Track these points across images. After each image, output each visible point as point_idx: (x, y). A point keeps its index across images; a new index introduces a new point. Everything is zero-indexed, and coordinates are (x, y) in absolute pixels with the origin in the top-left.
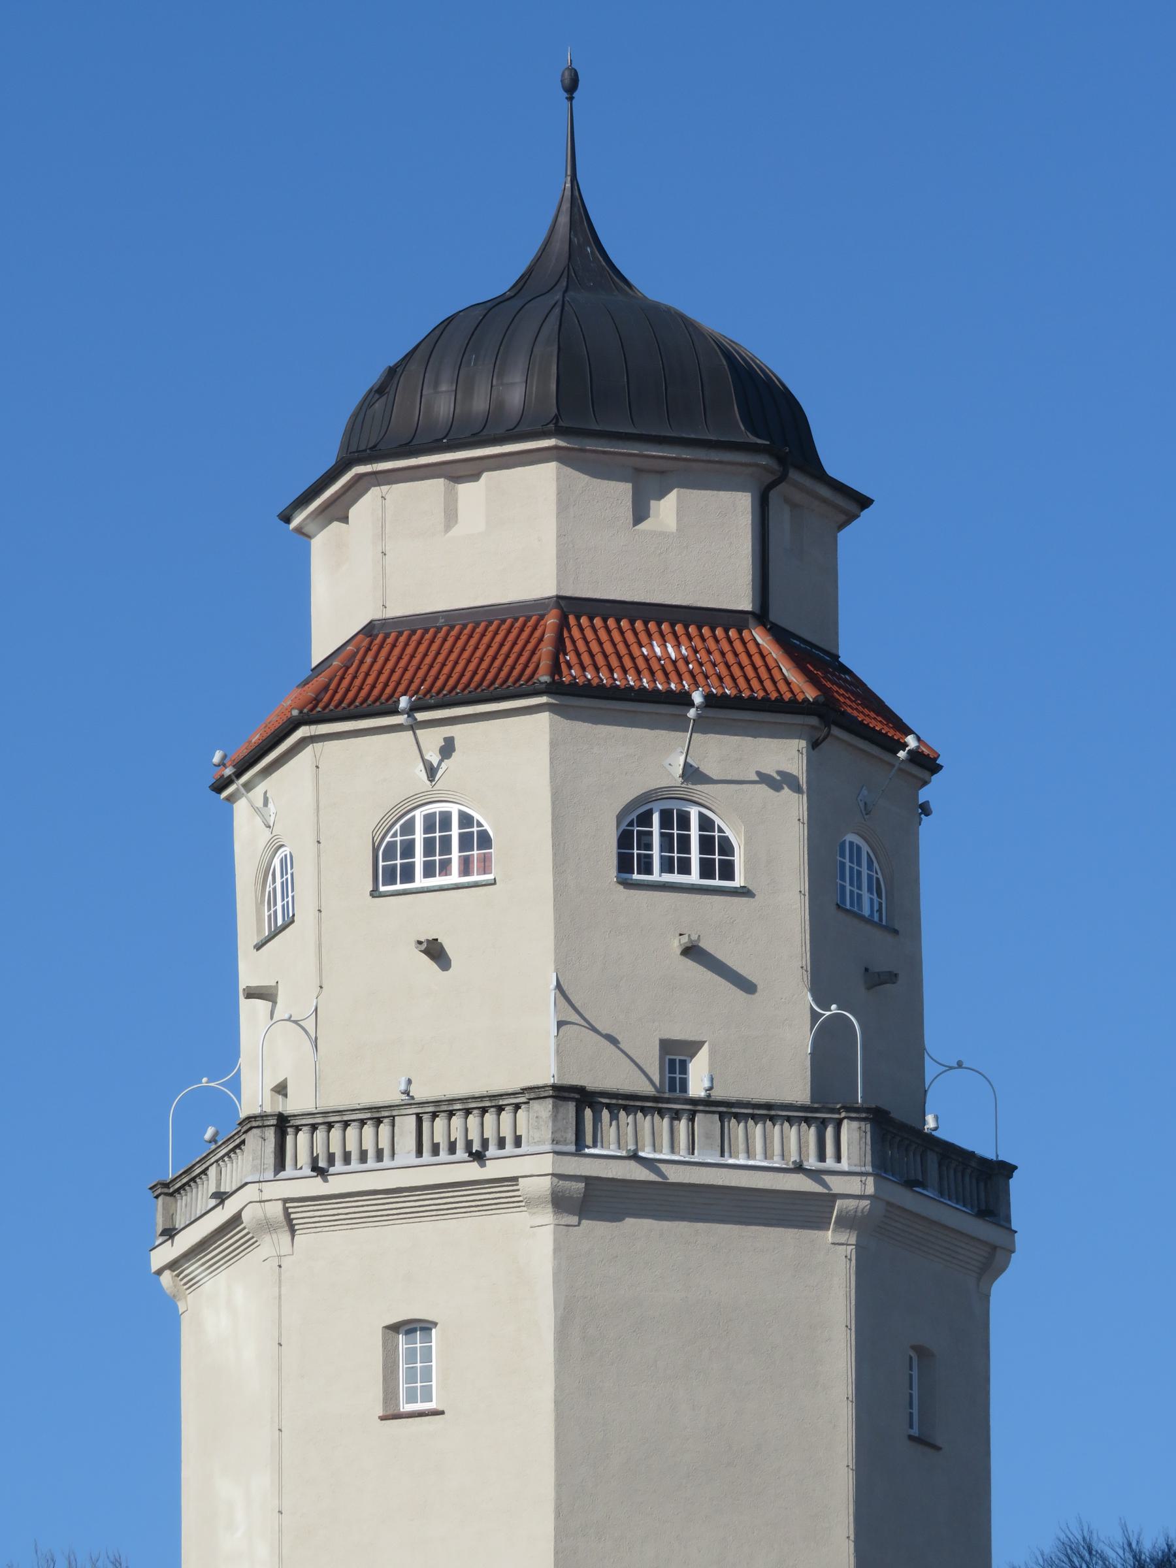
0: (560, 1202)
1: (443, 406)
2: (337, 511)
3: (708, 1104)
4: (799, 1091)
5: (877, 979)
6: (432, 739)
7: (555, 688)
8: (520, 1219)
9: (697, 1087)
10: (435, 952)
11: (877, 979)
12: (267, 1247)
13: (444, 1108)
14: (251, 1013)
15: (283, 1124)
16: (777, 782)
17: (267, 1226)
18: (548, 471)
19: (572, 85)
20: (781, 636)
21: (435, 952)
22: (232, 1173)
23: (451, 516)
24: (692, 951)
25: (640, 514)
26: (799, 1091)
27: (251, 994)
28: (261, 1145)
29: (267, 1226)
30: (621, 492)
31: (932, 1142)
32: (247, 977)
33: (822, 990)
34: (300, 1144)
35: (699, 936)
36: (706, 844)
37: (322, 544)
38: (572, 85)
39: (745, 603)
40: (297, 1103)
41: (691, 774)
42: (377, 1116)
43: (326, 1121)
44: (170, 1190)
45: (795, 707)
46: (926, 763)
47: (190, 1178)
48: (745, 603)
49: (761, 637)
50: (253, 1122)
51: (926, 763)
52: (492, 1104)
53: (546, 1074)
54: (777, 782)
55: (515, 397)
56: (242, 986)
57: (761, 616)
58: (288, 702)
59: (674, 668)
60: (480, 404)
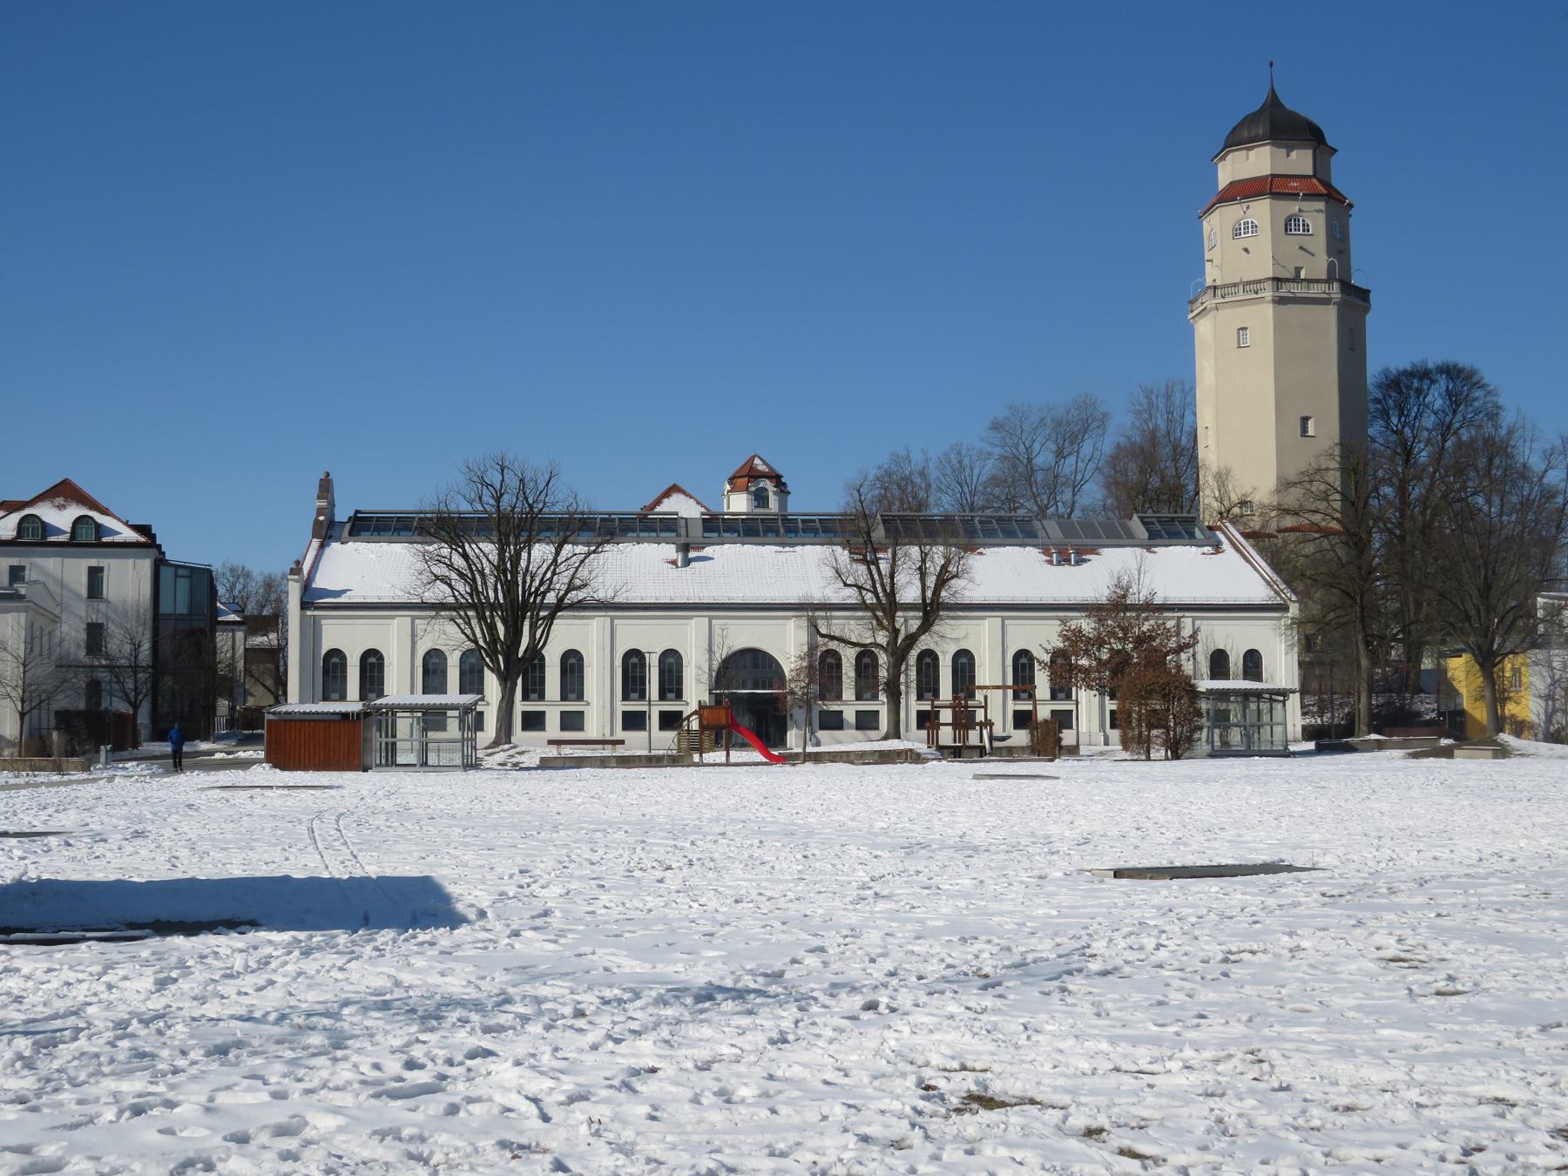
0: (1274, 302)
1: (1245, 134)
2: (1223, 158)
3: (1305, 280)
4: (1324, 276)
5: (1341, 252)
6: (1245, 205)
7: (1271, 193)
8: (1266, 305)
9: (1303, 276)
10: (1246, 250)
11: (1341, 252)
12: (1212, 314)
13: (1249, 283)
14: (1208, 265)
15: (1215, 288)
16: (1319, 211)
17: (1212, 309)
18: (1268, 147)
19: (1271, 65)
20: (1319, 180)
21: (1246, 250)
22: (1205, 298)
23: (1248, 158)
24: (1301, 248)
25: (1288, 156)
26: (1324, 276)
27: (95, 574)
28: (1211, 292)
29: (1212, 309)
30: (1283, 151)
31: (1353, 286)
32: (1206, 258)
33: (1329, 255)
34: (1219, 292)
35: (653, 1070)
37: (1220, 166)
38: (1271, 65)
39: (1310, 173)
40: (1218, 283)
41: (1300, 210)
42: (1235, 285)
43: (1224, 287)
44: (1191, 302)
45: (1322, 195)
46: (1351, 206)
47: (1195, 300)
48: (1310, 173)
49: (1314, 181)
50: (1209, 287)
51: (1351, 206)
52: (1259, 281)
53: (1271, 275)
54: (1319, 211)
55: (1261, 132)
56: (103, 563)
57: (1314, 176)
58: (1214, 198)
59: (1296, 188)
60: (1253, 134)
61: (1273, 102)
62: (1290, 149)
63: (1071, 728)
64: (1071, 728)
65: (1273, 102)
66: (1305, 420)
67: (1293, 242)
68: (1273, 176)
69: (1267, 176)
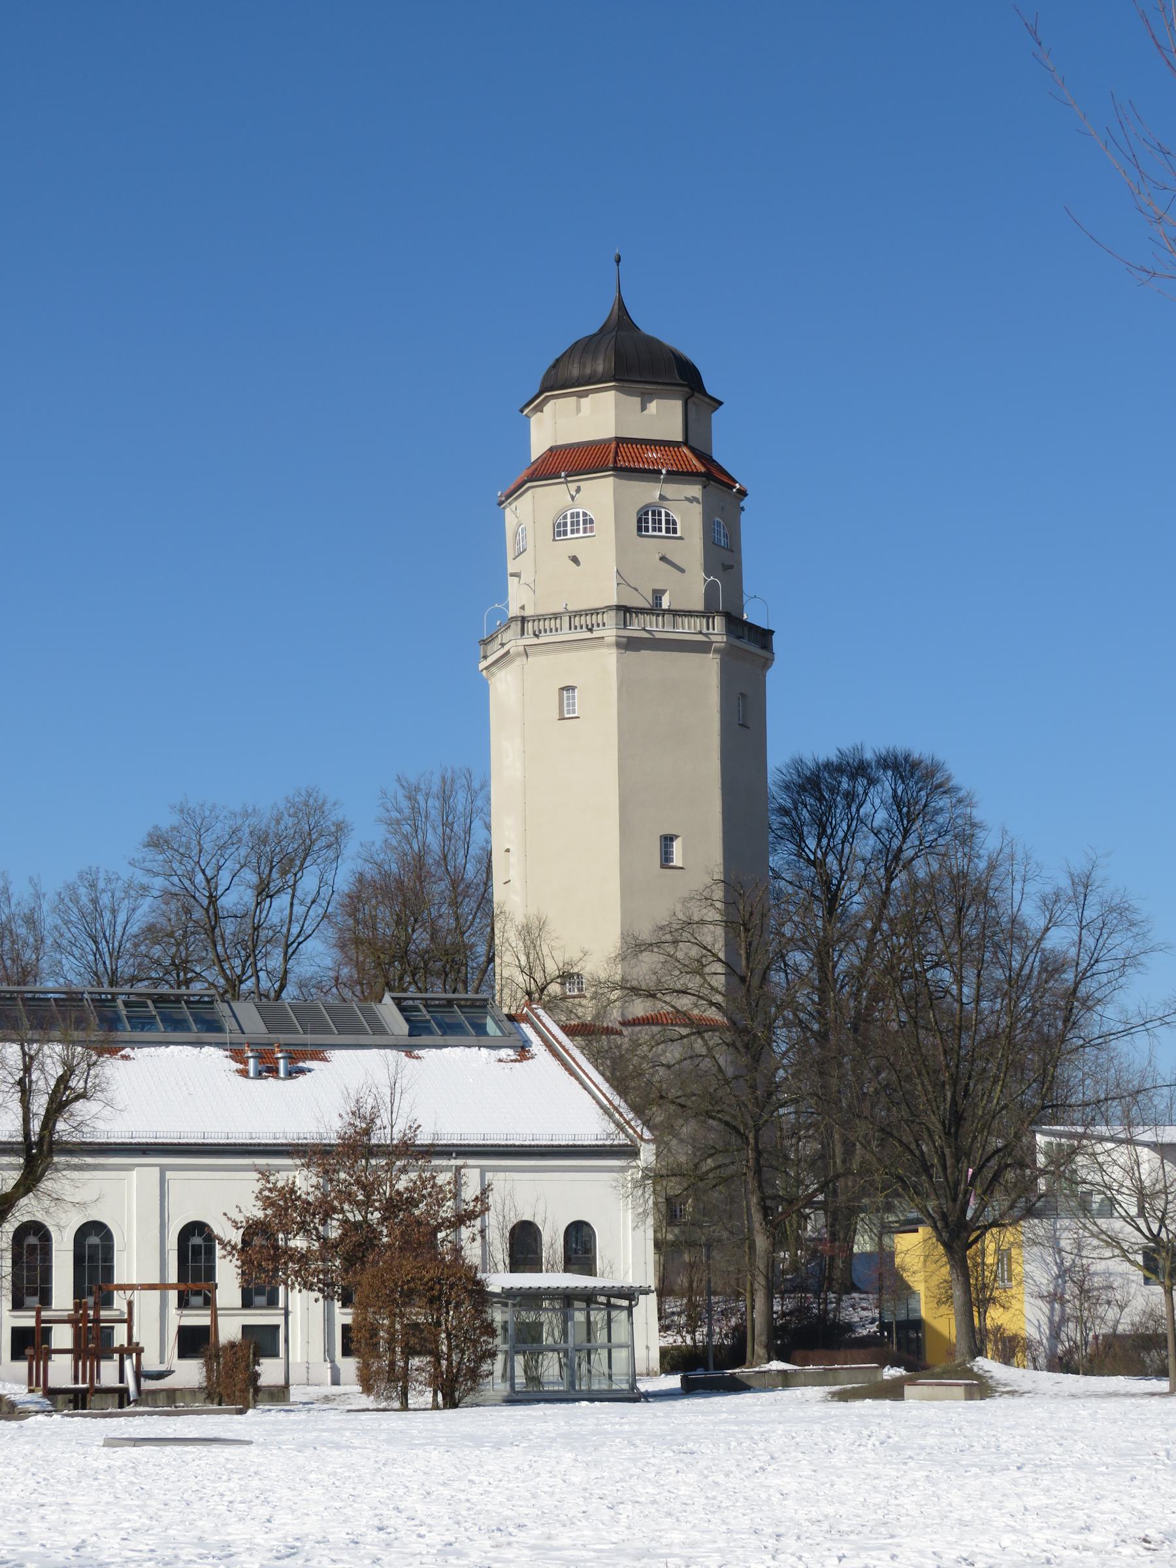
10: (575, 560)
14: (512, 581)
21: (575, 560)
23: (578, 410)
32: (512, 567)
34: (529, 626)
36: (667, 522)
61: (621, 320)
62: (646, 399)
63: (276, 1355)
64: (276, 1355)
65: (621, 320)
66: (667, 840)
67: (652, 547)
68: (620, 441)
69: (609, 441)
